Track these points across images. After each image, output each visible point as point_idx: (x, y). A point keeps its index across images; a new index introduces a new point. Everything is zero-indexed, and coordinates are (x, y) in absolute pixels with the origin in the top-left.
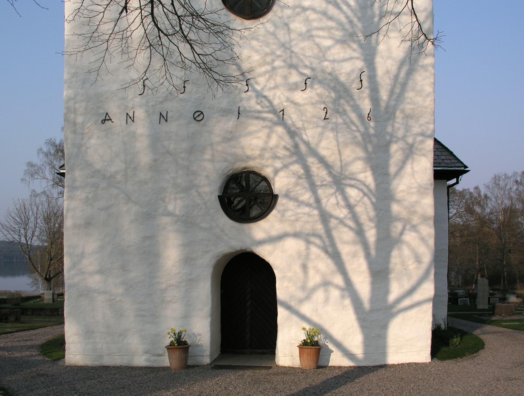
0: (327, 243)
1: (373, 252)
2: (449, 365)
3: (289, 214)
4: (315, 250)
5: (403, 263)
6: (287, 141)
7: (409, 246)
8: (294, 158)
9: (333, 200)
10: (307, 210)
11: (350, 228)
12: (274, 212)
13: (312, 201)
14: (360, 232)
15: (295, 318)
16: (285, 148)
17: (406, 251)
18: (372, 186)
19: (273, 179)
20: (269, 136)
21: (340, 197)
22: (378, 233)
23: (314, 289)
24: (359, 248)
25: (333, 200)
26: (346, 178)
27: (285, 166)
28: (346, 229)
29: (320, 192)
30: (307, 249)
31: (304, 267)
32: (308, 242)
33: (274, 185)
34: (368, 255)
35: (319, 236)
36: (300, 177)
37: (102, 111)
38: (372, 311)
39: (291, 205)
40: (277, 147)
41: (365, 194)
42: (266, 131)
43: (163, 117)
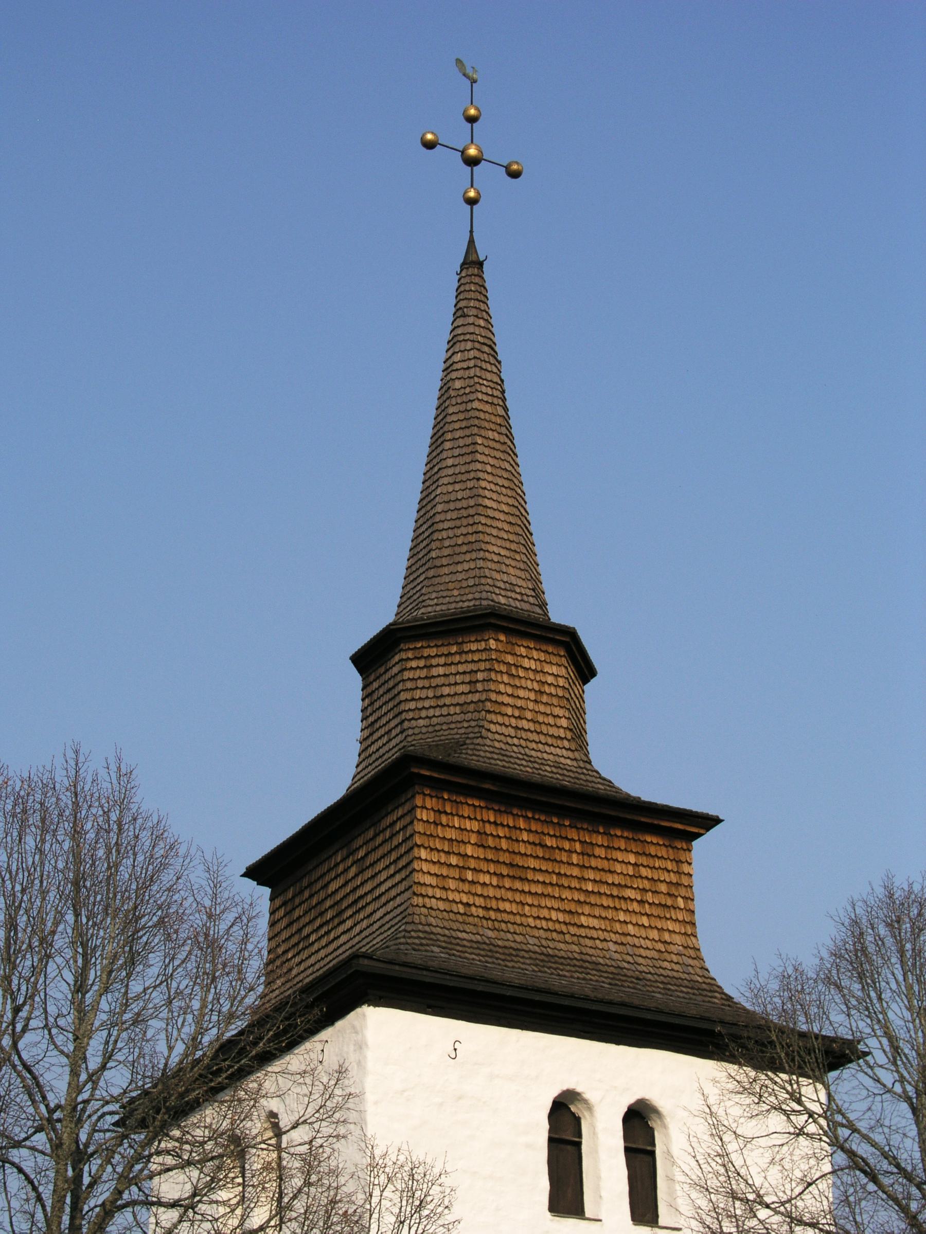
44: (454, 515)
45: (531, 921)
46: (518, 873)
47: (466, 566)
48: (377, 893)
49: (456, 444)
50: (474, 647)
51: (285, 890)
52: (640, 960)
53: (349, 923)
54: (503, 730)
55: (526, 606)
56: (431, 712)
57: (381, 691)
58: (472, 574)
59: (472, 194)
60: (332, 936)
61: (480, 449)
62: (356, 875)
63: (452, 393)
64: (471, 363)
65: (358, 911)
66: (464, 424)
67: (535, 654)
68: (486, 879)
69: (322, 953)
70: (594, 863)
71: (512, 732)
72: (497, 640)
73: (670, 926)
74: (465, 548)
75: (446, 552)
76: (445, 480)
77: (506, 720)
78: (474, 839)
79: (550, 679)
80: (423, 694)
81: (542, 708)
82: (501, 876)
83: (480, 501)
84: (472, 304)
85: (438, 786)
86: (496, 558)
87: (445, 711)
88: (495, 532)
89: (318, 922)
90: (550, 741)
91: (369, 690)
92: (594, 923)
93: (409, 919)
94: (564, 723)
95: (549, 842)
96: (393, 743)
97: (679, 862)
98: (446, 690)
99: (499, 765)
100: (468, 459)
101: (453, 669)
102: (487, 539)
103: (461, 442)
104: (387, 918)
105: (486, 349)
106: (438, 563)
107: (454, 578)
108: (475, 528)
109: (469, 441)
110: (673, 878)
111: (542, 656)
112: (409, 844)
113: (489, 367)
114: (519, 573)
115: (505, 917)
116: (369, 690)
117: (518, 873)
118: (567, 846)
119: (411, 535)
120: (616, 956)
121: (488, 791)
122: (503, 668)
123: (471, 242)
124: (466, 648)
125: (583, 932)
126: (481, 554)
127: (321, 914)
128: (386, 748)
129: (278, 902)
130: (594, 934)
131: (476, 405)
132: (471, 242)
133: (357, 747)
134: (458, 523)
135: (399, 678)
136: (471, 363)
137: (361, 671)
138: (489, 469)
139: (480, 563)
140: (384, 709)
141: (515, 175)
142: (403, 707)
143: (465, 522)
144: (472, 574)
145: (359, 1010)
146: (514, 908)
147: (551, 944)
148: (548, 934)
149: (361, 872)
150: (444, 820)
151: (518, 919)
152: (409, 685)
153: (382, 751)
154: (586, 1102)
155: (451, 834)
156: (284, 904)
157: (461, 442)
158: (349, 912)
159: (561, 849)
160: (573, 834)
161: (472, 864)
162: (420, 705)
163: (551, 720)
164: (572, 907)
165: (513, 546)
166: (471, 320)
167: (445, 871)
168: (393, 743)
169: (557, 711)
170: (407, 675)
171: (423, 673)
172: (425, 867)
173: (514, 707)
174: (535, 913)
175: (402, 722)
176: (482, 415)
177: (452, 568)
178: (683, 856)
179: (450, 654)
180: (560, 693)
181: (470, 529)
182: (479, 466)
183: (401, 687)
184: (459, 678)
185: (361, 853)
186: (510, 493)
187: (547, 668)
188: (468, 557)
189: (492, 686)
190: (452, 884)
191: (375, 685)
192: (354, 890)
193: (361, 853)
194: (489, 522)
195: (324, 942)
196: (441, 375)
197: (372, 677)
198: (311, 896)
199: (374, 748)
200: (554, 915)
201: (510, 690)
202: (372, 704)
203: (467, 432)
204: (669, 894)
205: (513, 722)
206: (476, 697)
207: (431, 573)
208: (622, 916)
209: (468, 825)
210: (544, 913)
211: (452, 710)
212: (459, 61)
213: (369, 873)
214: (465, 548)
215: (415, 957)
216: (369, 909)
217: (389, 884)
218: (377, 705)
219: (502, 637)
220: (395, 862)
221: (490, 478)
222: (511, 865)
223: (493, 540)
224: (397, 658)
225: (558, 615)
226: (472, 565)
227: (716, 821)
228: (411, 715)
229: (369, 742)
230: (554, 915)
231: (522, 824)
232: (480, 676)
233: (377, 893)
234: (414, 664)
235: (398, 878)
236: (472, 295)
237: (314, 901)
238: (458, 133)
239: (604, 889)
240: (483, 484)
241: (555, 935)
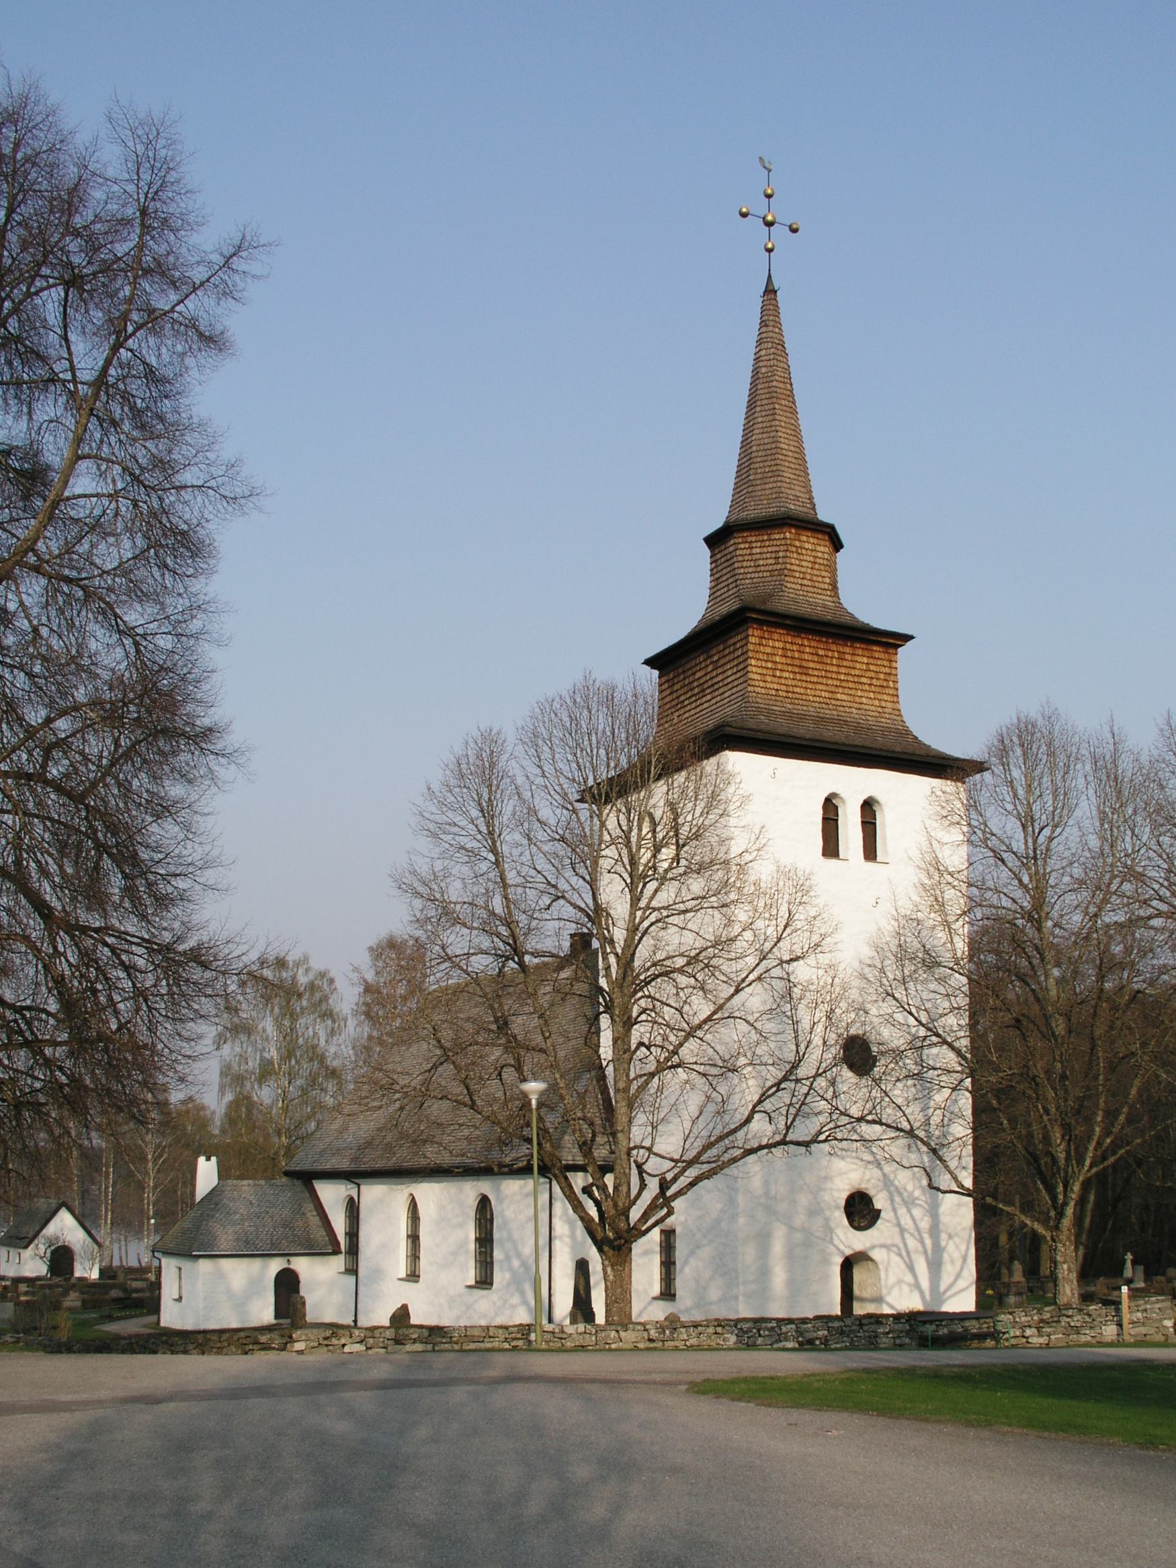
1: (930, 1252)
44: (763, 453)
45: (811, 698)
46: (805, 671)
47: (771, 486)
48: (726, 682)
49: (763, 408)
50: (777, 536)
51: (668, 674)
52: (869, 718)
53: (709, 697)
54: (794, 586)
55: (805, 510)
56: (753, 575)
57: (723, 560)
58: (774, 490)
59: (770, 246)
60: (698, 703)
61: (777, 411)
62: (713, 670)
63: (761, 376)
64: (772, 357)
65: (715, 691)
66: (768, 396)
67: (811, 540)
68: (786, 675)
69: (693, 712)
70: (845, 663)
71: (799, 587)
72: (790, 532)
73: (885, 697)
74: (770, 474)
75: (759, 476)
76: (757, 431)
77: (796, 580)
78: (780, 652)
79: (820, 555)
80: (748, 564)
81: (815, 572)
82: (795, 673)
83: (778, 445)
84: (771, 318)
85: (761, 623)
86: (788, 480)
87: (761, 575)
88: (787, 464)
89: (689, 694)
90: (820, 591)
91: (714, 558)
92: (844, 697)
93: (746, 700)
94: (827, 580)
95: (821, 652)
96: (731, 592)
97: (891, 661)
98: (761, 562)
99: (793, 609)
100: (770, 418)
101: (765, 550)
102: (783, 468)
103: (766, 407)
104: (733, 697)
105: (780, 347)
106: (754, 483)
107: (764, 492)
108: (776, 462)
109: (771, 407)
110: (887, 670)
111: (816, 541)
112: (745, 656)
113: (781, 359)
114: (800, 489)
115: (797, 696)
116: (714, 558)
117: (805, 671)
118: (830, 654)
119: (736, 463)
120: (857, 716)
121: (790, 625)
122: (794, 549)
123: (770, 277)
124: (773, 537)
125: (838, 703)
126: (780, 478)
127: (692, 690)
128: (727, 595)
129: (663, 679)
130: (845, 704)
131: (774, 383)
132: (770, 277)
133: (708, 592)
134: (766, 458)
135: (734, 554)
136: (772, 357)
137: (709, 547)
138: (783, 424)
139: (779, 484)
140: (724, 571)
141: (794, 231)
142: (737, 571)
143: (769, 458)
144: (774, 490)
145: (724, 753)
146: (802, 691)
147: (822, 711)
148: (820, 705)
149: (716, 668)
150: (764, 642)
151: (804, 697)
152: (740, 558)
153: (723, 596)
154: (841, 798)
155: (768, 650)
156: (668, 681)
157: (766, 407)
158: (708, 691)
159: (827, 656)
160: (834, 647)
161: (779, 667)
162: (746, 570)
163: (820, 579)
164: (833, 689)
165: (798, 472)
166: (771, 329)
167: (765, 672)
168: (731, 592)
169: (824, 574)
170: (738, 552)
171: (748, 552)
172: (754, 669)
173: (800, 572)
174: (813, 692)
175: (736, 581)
176: (778, 390)
177: (763, 487)
178: (893, 658)
179: (763, 541)
180: (826, 563)
181: (773, 463)
182: (777, 423)
183: (735, 559)
184: (768, 555)
185: (715, 658)
186: (795, 439)
187: (818, 548)
188: (772, 480)
189: (788, 560)
190: (769, 679)
191: (718, 556)
192: (712, 678)
193: (715, 658)
194: (783, 458)
195: (693, 705)
196: (752, 362)
197: (717, 551)
198: (684, 679)
199: (718, 593)
200: (823, 694)
201: (797, 562)
202: (716, 567)
203: (770, 401)
204: (885, 680)
205: (800, 581)
206: (779, 567)
207: (750, 489)
208: (859, 693)
209: (777, 644)
210: (818, 693)
211: (765, 574)
212: (761, 158)
213: (720, 670)
214: (770, 474)
215: (751, 724)
216: (721, 691)
217: (733, 678)
218: (720, 568)
219: (793, 531)
220: (737, 665)
221: (784, 430)
222: (800, 667)
223: (786, 469)
224: (732, 542)
225: (824, 516)
226: (775, 485)
227: (912, 637)
228: (741, 577)
229: (715, 589)
230: (823, 694)
231: (806, 643)
232: (781, 554)
233: (726, 682)
234: (742, 546)
235: (738, 675)
236: (771, 312)
237: (687, 682)
238: (759, 207)
239: (850, 678)
240: (780, 434)
241: (824, 705)
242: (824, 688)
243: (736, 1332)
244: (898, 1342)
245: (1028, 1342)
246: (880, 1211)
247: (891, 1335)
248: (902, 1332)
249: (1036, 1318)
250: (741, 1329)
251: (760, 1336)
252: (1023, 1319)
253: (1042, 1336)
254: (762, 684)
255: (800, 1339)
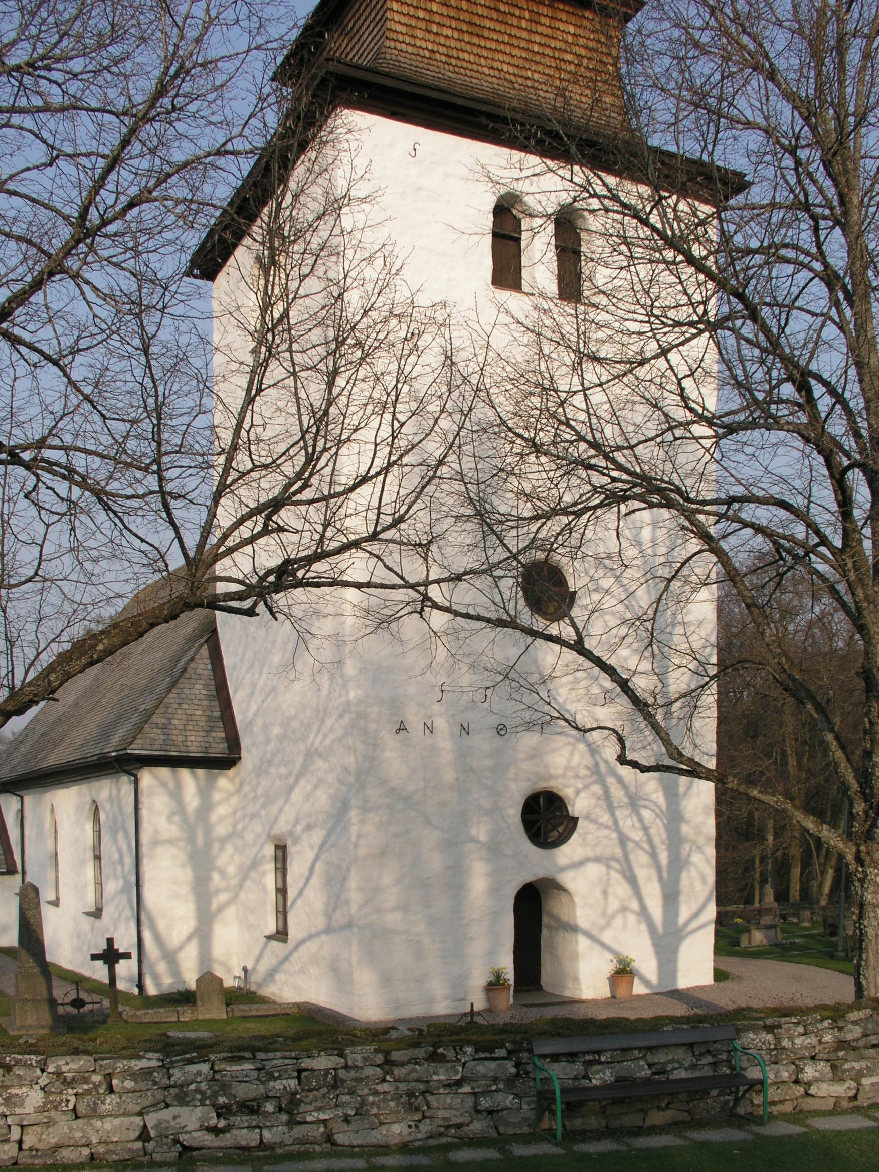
0: (625, 867)
1: (665, 875)
2: (721, 985)
3: (590, 837)
4: (615, 876)
5: (692, 885)
6: (588, 760)
7: (696, 867)
8: (594, 778)
9: (629, 823)
10: (606, 832)
11: (647, 852)
12: (575, 836)
13: (610, 823)
14: (654, 855)
15: (597, 948)
16: (587, 768)
17: (694, 873)
18: (664, 806)
19: (574, 800)
20: (572, 754)
21: (635, 819)
22: (670, 856)
23: (613, 916)
24: (653, 872)
25: (629, 823)
26: (641, 799)
27: (586, 787)
28: (641, 852)
29: (618, 813)
30: (608, 874)
31: (605, 893)
32: (609, 867)
33: (573, 806)
34: (660, 878)
35: (618, 860)
36: (599, 799)
37: (396, 719)
38: (666, 935)
39: (591, 827)
40: (579, 766)
41: (657, 816)
42: (569, 748)
43: (465, 730)
45: (486, 70)
46: (476, 30)
68: (448, 32)
70: (540, 29)
82: (461, 31)
115: (464, 64)
117: (476, 30)
118: (517, 12)
151: (475, 67)
159: (513, 15)
161: (437, 18)
167: (413, 22)
172: (397, 17)
190: (419, 34)
230: (505, 67)
239: (547, 51)
242: (507, 59)
243: (43, 1081)
244: (485, 1103)
245: (807, 1094)
246: (577, 819)
247: (467, 1089)
248: (495, 1080)
249: (828, 1038)
250: (58, 1074)
251: (111, 1090)
252: (798, 1041)
253: (842, 1080)
254: (408, 40)
255: (222, 1100)
